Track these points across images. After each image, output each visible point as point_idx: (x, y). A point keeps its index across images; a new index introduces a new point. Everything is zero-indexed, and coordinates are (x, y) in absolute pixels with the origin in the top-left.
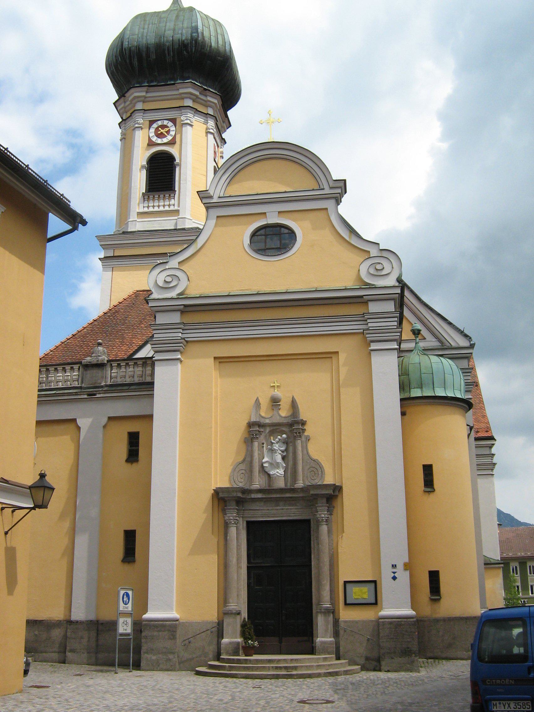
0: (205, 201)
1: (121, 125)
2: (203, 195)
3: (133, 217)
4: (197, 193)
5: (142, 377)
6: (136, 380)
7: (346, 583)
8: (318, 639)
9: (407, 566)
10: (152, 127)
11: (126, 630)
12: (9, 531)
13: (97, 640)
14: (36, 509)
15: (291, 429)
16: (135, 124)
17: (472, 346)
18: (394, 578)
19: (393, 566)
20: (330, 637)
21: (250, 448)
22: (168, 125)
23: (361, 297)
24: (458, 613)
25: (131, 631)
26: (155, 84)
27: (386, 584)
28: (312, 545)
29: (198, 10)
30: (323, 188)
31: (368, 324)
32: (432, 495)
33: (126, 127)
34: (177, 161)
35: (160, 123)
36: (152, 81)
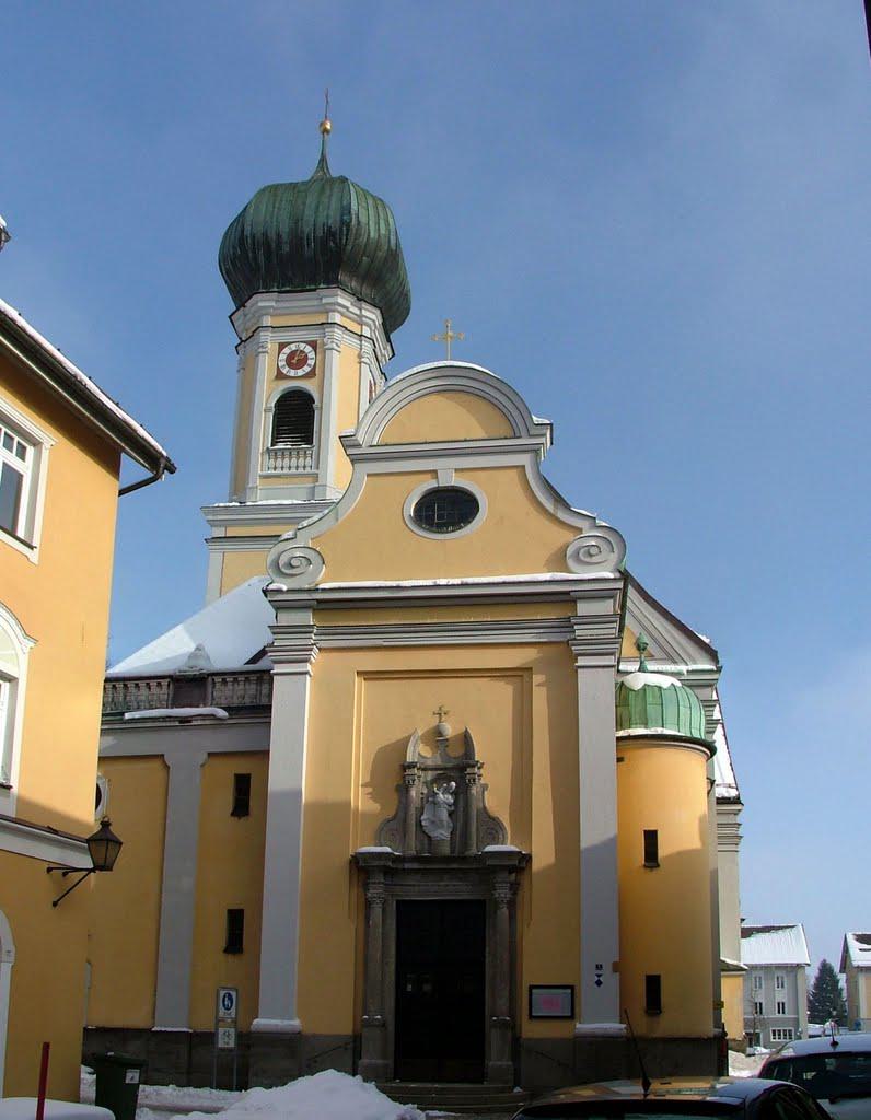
2: (347, 442)
3: (255, 480)
6: (247, 701)
9: (616, 967)
17: (719, 670)
18: (599, 983)
21: (404, 800)
23: (568, 593)
27: (588, 995)
32: (655, 871)
35: (293, 347)
36: (283, 286)
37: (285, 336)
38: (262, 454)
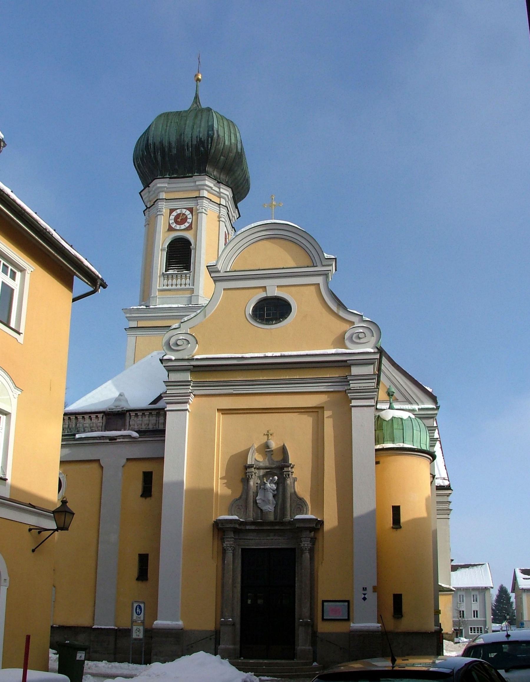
0: (213, 275)
1: (145, 212)
2: (212, 269)
4: (206, 267)
5: (156, 425)
6: (151, 427)
7: (323, 601)
8: (299, 647)
10: (172, 214)
11: (139, 636)
12: (36, 548)
13: (116, 644)
14: (59, 531)
15: (281, 472)
16: (157, 212)
17: (438, 408)
18: (364, 599)
19: (363, 588)
20: (309, 646)
22: (186, 213)
23: (345, 361)
24: (416, 627)
25: (143, 637)
26: (175, 176)
28: (296, 570)
29: (215, 110)
30: (316, 265)
31: (350, 385)
33: (150, 212)
34: (193, 245)
35: (179, 211)
36: (173, 174)
37: (173, 205)
38: (160, 277)
